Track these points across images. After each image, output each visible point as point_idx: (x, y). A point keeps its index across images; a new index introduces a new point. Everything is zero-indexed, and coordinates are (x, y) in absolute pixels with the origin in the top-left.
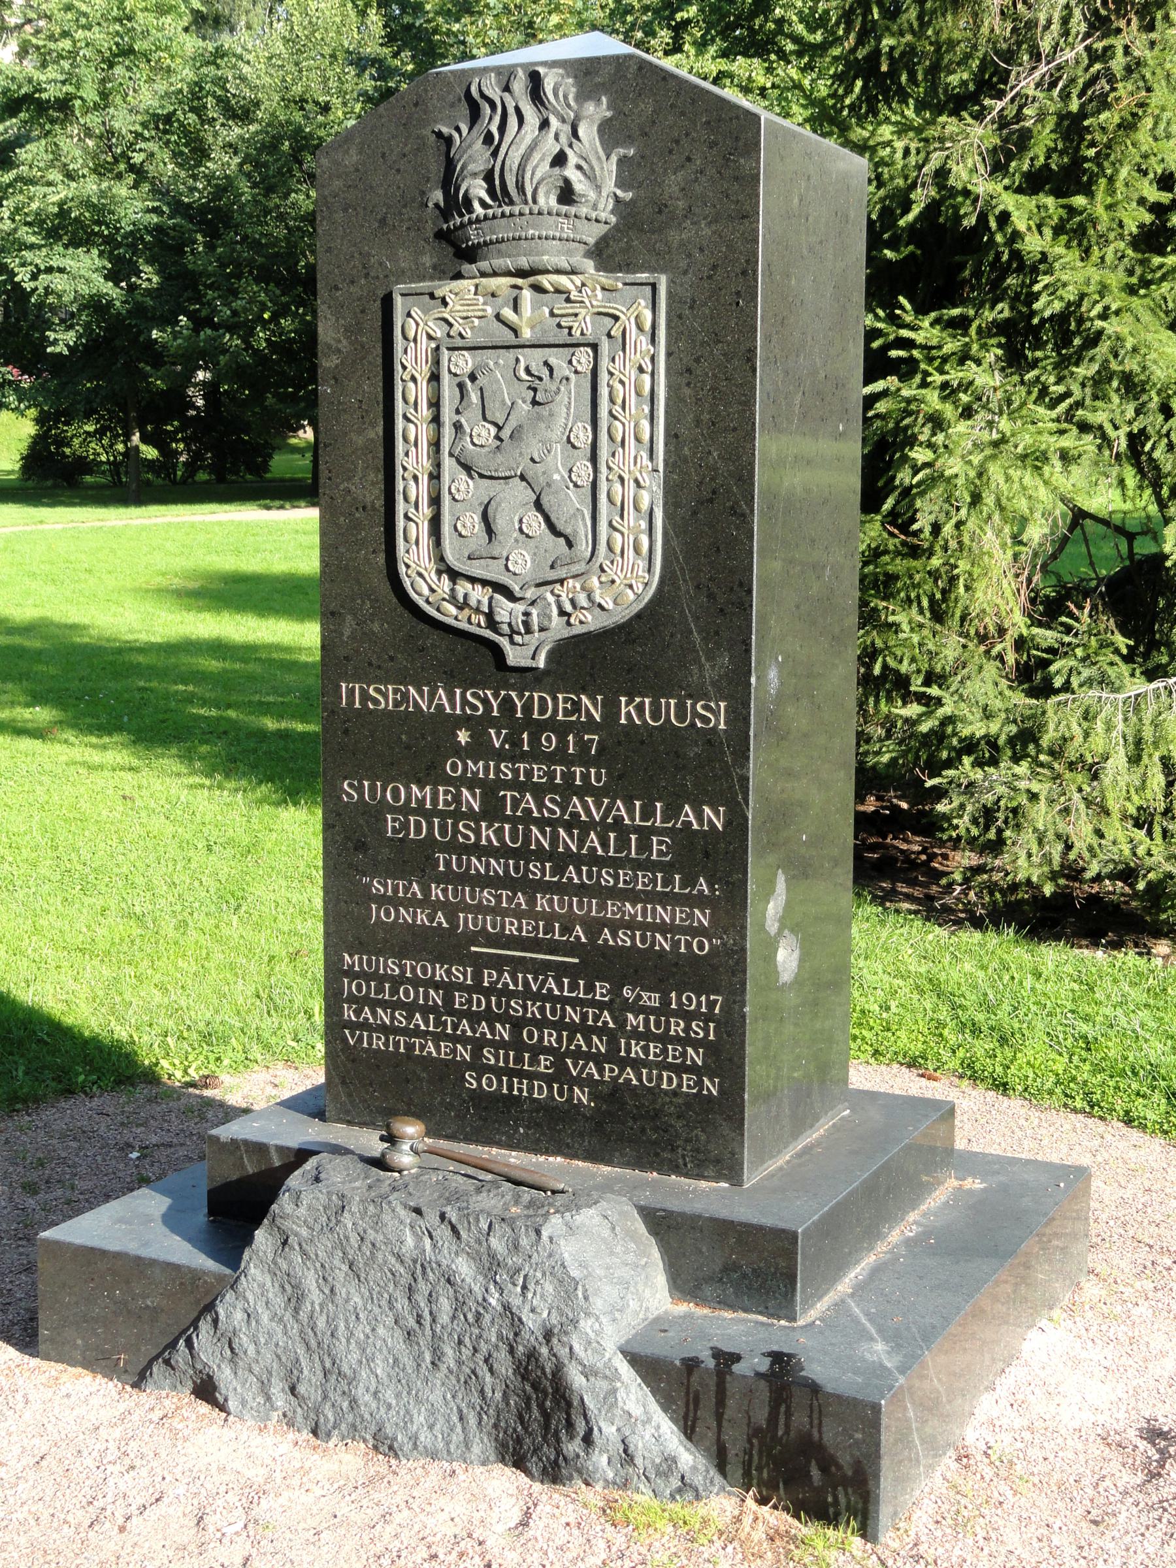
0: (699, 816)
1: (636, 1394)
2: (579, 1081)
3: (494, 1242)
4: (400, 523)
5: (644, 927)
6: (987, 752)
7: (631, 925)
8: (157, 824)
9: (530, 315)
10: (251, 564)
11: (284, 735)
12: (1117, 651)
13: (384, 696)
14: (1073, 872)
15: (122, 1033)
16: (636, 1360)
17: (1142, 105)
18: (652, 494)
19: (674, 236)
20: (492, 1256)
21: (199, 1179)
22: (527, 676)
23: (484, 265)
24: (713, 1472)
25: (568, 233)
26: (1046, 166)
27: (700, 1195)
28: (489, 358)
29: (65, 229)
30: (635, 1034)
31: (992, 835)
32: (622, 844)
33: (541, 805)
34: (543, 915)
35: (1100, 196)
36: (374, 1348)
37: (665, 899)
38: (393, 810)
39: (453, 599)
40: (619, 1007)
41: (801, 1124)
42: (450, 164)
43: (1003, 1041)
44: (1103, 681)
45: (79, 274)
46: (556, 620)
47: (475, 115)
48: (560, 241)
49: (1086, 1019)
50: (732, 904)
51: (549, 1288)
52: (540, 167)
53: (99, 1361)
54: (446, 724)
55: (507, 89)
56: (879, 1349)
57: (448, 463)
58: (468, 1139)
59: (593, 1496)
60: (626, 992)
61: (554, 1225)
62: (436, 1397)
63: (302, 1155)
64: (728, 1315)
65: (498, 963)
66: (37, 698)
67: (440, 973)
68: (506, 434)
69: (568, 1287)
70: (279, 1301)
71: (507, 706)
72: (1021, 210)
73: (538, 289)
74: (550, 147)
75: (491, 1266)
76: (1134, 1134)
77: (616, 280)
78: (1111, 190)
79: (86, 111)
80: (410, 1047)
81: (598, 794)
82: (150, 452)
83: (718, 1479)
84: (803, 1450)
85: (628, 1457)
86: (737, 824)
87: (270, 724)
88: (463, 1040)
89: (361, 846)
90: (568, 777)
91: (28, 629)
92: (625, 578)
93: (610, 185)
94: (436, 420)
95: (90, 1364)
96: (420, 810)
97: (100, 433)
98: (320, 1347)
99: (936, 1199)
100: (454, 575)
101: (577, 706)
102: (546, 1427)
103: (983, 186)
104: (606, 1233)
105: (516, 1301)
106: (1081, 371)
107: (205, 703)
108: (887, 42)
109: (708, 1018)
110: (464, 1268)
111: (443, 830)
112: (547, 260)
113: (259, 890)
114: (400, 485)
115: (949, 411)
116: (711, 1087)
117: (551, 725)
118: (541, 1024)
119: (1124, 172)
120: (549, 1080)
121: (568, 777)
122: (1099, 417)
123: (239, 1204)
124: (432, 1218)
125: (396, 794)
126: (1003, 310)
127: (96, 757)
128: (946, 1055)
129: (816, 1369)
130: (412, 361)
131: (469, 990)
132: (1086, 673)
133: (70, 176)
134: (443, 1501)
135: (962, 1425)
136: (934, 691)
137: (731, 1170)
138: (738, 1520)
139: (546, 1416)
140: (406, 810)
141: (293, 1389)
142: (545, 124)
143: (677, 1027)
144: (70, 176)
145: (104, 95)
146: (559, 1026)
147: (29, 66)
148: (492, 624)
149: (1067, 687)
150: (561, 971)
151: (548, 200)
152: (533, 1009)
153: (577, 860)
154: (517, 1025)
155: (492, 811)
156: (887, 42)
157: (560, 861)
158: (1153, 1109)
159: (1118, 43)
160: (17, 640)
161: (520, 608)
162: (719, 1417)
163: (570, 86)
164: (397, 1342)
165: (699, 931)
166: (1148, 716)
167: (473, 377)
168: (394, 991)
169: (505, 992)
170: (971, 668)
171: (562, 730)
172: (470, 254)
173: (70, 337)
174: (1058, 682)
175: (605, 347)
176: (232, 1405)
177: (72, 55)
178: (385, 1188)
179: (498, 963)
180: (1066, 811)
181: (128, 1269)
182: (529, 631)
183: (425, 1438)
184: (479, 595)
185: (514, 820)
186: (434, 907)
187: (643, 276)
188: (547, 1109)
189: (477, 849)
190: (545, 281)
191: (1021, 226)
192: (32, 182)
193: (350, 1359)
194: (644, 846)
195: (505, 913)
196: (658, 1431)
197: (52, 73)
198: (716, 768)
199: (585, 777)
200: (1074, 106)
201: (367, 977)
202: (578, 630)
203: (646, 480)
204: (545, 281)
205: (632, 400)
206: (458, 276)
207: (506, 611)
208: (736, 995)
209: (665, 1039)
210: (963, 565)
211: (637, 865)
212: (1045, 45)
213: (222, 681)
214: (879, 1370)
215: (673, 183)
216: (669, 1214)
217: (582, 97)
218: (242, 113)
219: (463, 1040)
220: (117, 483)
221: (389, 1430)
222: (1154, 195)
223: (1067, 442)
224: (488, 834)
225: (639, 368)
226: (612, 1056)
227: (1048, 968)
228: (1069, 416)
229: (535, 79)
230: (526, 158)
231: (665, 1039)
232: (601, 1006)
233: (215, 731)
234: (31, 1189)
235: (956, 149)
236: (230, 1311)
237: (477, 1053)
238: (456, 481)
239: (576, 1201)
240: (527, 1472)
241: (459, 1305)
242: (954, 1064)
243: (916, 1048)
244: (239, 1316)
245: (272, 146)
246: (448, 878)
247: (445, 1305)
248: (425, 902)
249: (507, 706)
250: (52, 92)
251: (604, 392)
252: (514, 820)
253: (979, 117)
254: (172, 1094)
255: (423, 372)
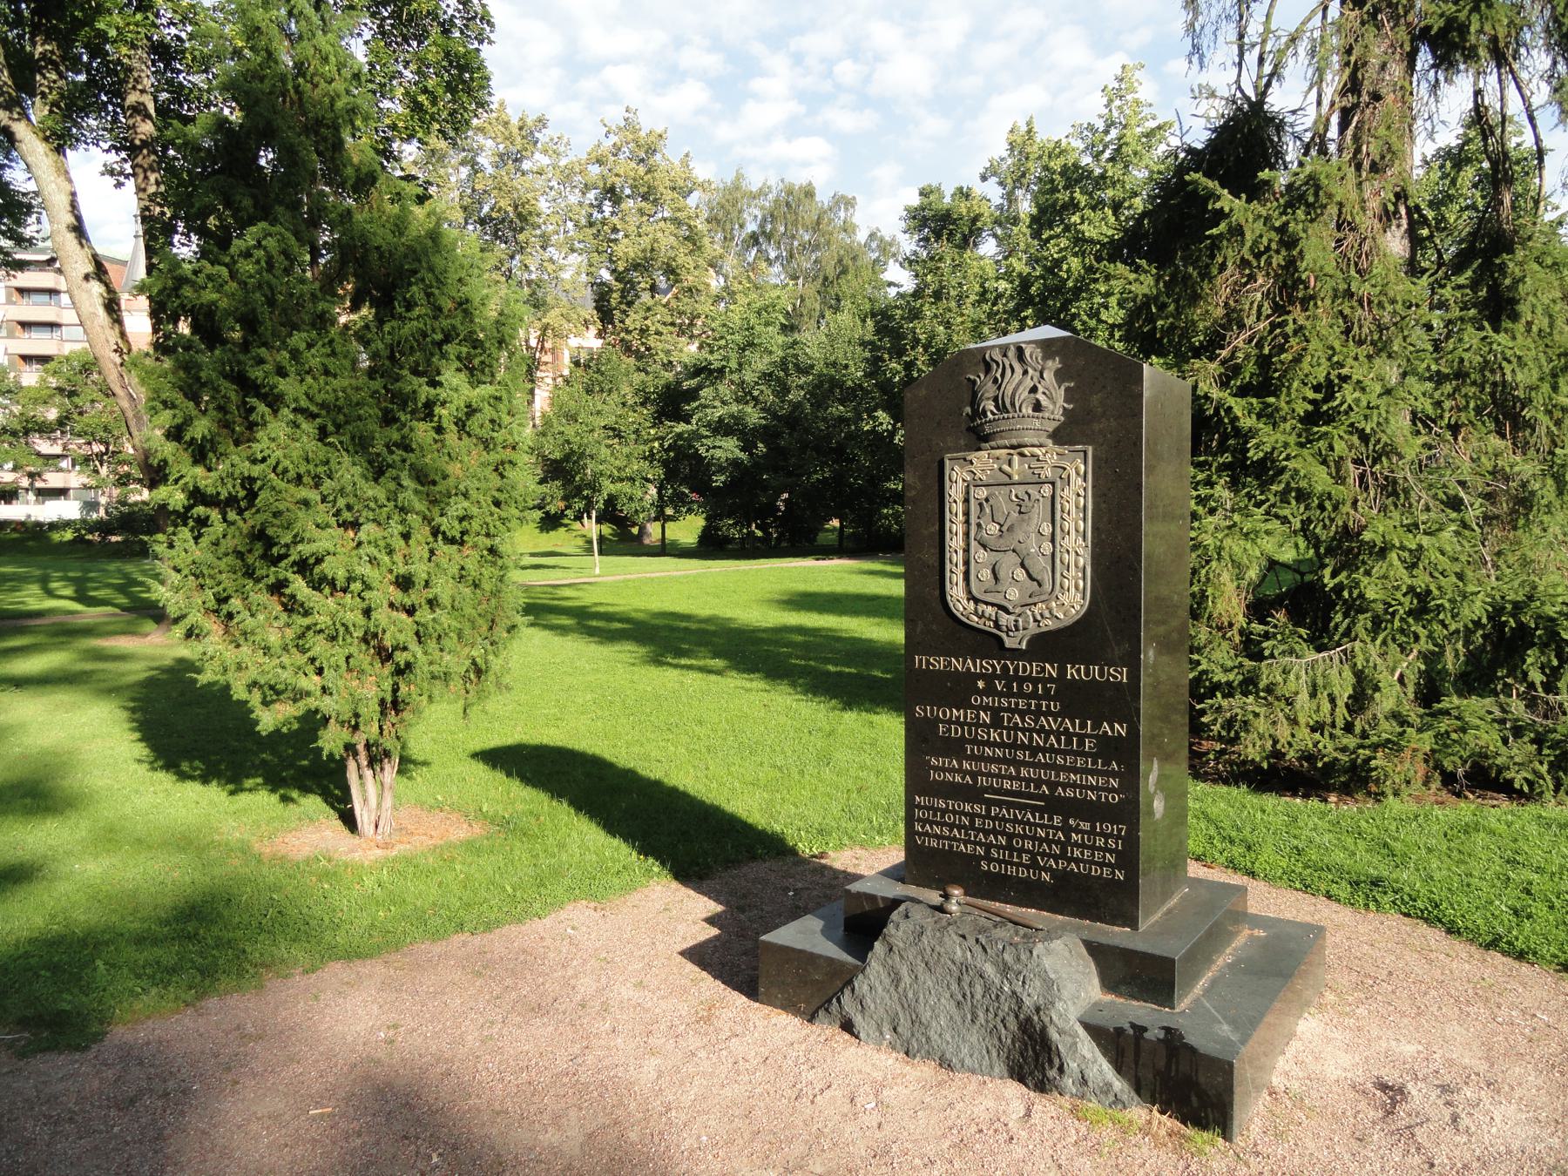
0: (1112, 729)
1: (1087, 1047)
2: (1045, 869)
3: (1006, 956)
4: (948, 574)
5: (1081, 787)
6: (1229, 690)
7: (1074, 786)
8: (782, 719)
9: (1017, 468)
10: (812, 588)
11: (839, 674)
12: (1301, 637)
13: (939, 663)
14: (1277, 754)
15: (778, 828)
16: (1087, 1027)
17: (1305, 349)
18: (1085, 559)
19: (1096, 427)
20: (1005, 964)
21: (838, 909)
22: (1015, 654)
23: (993, 443)
24: (1133, 1094)
25: (1038, 425)
26: (1250, 383)
27: (1116, 935)
28: (996, 490)
29: (722, 428)
30: (1076, 844)
31: (1232, 734)
32: (1069, 742)
33: (1023, 721)
34: (1024, 779)
35: (1283, 397)
36: (939, 1011)
37: (1093, 772)
38: (942, 722)
39: (976, 613)
40: (1067, 830)
41: (1166, 895)
42: (975, 394)
43: (1249, 848)
44: (1291, 652)
45: (728, 448)
46: (1032, 624)
47: (988, 369)
48: (1034, 429)
49: (1295, 837)
50: (1131, 780)
51: (1038, 984)
52: (1023, 394)
53: (789, 1006)
54: (972, 677)
55: (1005, 355)
56: (1226, 1028)
57: (973, 543)
58: (982, 898)
59: (1066, 1102)
60: (1071, 822)
61: (1039, 948)
62: (974, 1039)
63: (895, 903)
64: (1135, 1003)
65: (999, 804)
66: (716, 655)
67: (968, 808)
68: (1005, 529)
69: (1049, 984)
70: (887, 981)
71: (1005, 668)
72: (1238, 406)
73: (1022, 455)
74: (1029, 383)
75: (1004, 969)
76: (1335, 906)
77: (1065, 450)
78: (1289, 394)
79: (731, 372)
80: (951, 847)
81: (1055, 716)
82: (759, 533)
83: (1136, 1097)
84: (1192, 1088)
85: (1084, 1081)
86: (1134, 732)
87: (831, 668)
88: (980, 844)
89: (925, 740)
90: (1039, 706)
91: (708, 620)
92: (1071, 600)
93: (1061, 402)
94: (967, 522)
95: (784, 1008)
96: (957, 722)
97: (735, 524)
98: (910, 1008)
99: (1240, 940)
100: (977, 601)
101: (1043, 669)
102: (1037, 1060)
103: (1215, 393)
104: (1067, 954)
105: (1019, 990)
106: (1274, 488)
107: (797, 657)
108: (1160, 323)
109: (1119, 837)
110: (989, 969)
111: (970, 733)
112: (1027, 440)
113: (838, 755)
114: (948, 555)
115: (1200, 510)
116: (1120, 875)
117: (1029, 679)
118: (1023, 837)
119: (1295, 384)
120: (1028, 867)
121: (1039, 706)
122: (1286, 512)
123: (864, 924)
124: (971, 941)
125: (944, 714)
126: (1227, 458)
127: (748, 685)
128: (1217, 855)
129: (1192, 1039)
130: (955, 492)
131: (984, 817)
132: (1282, 648)
133: (724, 403)
134: (981, 1099)
135: (1271, 1074)
136: (1195, 657)
137: (1133, 923)
138: (1149, 1122)
139: (1037, 1055)
140: (950, 722)
141: (895, 1030)
142: (1025, 372)
143: (1100, 842)
144: (724, 403)
145: (740, 365)
146: (1034, 838)
147: (705, 354)
148: (997, 626)
149: (1272, 656)
150: (1034, 809)
151: (1027, 410)
152: (1019, 829)
153: (1044, 750)
154: (1010, 837)
155: (997, 723)
156: (1160, 323)
157: (1034, 750)
158: (1343, 890)
159: (1290, 318)
160: (703, 626)
161: (1012, 618)
162: (1136, 1063)
163: (1039, 353)
164: (953, 1010)
165: (1113, 790)
166: (1319, 672)
167: (987, 500)
168: (943, 817)
169: (1003, 819)
170: (1215, 644)
171: (1035, 681)
172: (986, 438)
173: (723, 478)
174: (1267, 653)
175: (1059, 484)
176: (862, 1035)
177: (726, 346)
178: (944, 923)
179: (999, 804)
180: (1274, 723)
181: (809, 959)
182: (1017, 629)
183: (968, 1061)
184: (989, 610)
185: (1008, 729)
186: (964, 773)
187: (1079, 447)
188: (1026, 882)
189: (988, 743)
190: (1026, 451)
191: (1239, 414)
192: (706, 407)
193: (926, 1015)
194: (1081, 743)
195: (1003, 777)
196: (1102, 1069)
197: (716, 356)
198: (1122, 702)
199: (1048, 706)
200: (1266, 351)
201: (928, 808)
202: (1044, 629)
203: (1081, 551)
204: (1026, 451)
205: (1073, 510)
206: (979, 449)
207: (1005, 619)
208: (1134, 827)
209: (1093, 848)
210: (1210, 591)
211: (1076, 754)
212: (1248, 322)
213: (805, 646)
214: (1227, 1042)
215: (1095, 399)
216: (1100, 945)
217: (1045, 358)
218: (804, 370)
219: (980, 844)
220: (743, 548)
221: (948, 1056)
222: (1311, 395)
223: (1269, 526)
224: (994, 735)
225: (1077, 493)
226: (1063, 855)
227: (1269, 809)
228: (1267, 513)
229: (1020, 351)
230: (1015, 390)
231: (1093, 848)
232: (1057, 828)
233: (804, 672)
234: (742, 909)
235: (1201, 376)
236: (860, 984)
237: (988, 852)
238: (981, 555)
239: (1050, 936)
240: (1027, 1086)
241: (987, 989)
242: (1222, 860)
243: (1200, 851)
244: (866, 987)
245: (819, 386)
246: (972, 758)
247: (979, 989)
248: (960, 771)
249: (1005, 668)
250: (716, 365)
251: (1058, 507)
252: (1008, 729)
253: (1211, 359)
254: (804, 861)
255: (960, 497)
